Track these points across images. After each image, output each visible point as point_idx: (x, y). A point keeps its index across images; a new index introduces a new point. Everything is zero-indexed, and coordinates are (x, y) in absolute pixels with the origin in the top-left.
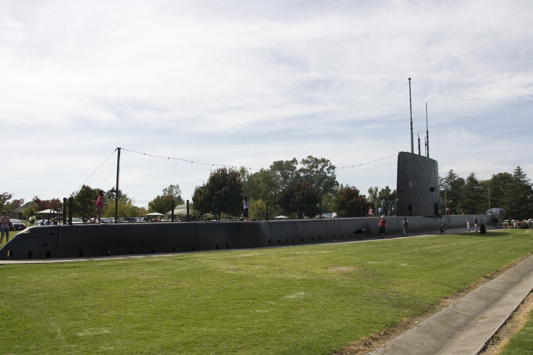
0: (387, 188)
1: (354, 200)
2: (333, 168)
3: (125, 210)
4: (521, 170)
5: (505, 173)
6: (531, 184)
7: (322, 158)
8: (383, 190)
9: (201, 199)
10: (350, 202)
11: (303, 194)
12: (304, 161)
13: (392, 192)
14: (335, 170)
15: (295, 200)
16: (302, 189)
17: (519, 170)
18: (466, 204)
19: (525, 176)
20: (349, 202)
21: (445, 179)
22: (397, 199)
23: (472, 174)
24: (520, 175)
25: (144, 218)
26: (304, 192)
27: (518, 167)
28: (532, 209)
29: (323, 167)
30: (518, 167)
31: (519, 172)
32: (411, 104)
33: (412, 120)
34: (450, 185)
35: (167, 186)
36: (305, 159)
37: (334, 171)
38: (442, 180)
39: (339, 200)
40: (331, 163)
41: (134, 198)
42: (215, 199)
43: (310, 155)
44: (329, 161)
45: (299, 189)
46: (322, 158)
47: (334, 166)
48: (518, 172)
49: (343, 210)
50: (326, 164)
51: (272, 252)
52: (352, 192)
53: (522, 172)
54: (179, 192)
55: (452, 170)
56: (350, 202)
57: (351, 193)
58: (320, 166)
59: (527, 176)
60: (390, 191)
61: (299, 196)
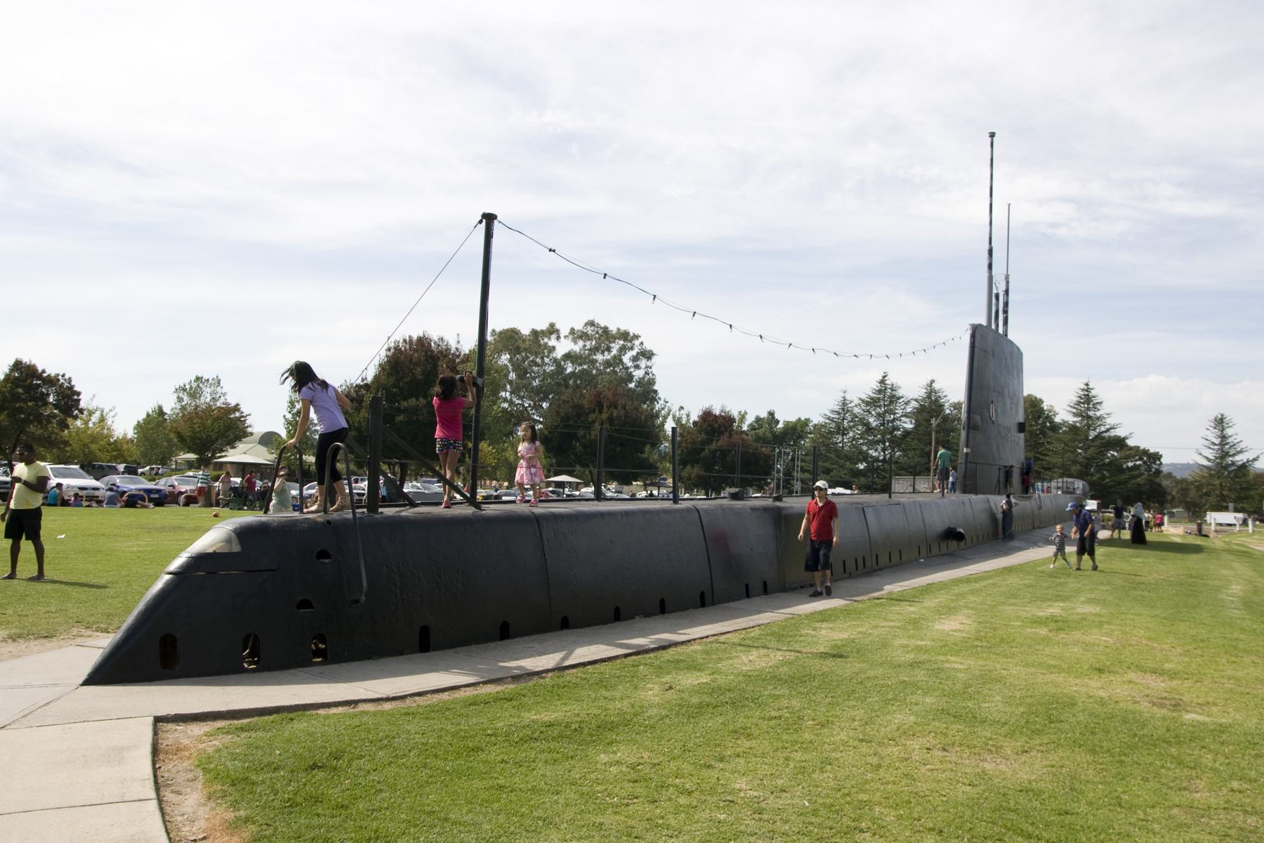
0: (771, 414)
1: (723, 442)
2: (648, 355)
3: (92, 442)
4: (1092, 391)
6: (1109, 424)
7: (618, 329)
8: (758, 419)
9: (362, 420)
10: (713, 446)
11: (611, 420)
12: (574, 333)
13: (780, 425)
16: (607, 407)
17: (1087, 391)
19: (1098, 407)
20: (710, 447)
21: (916, 400)
22: (967, 446)
24: (1088, 404)
25: (126, 466)
26: (615, 414)
27: (1087, 385)
28: (1110, 484)
29: (623, 350)
30: (1087, 385)
31: (1088, 395)
32: (991, 201)
33: (993, 245)
35: (186, 379)
36: (579, 326)
37: (649, 364)
38: (907, 403)
39: (684, 439)
40: (642, 343)
41: (114, 408)
42: (401, 422)
43: (591, 319)
44: (637, 337)
45: (600, 406)
46: (618, 329)
47: (650, 351)
48: (1084, 395)
50: (629, 344)
52: (719, 422)
53: (1094, 397)
54: (220, 397)
55: (933, 381)
56: (713, 446)
57: (717, 422)
58: (615, 348)
59: (1104, 405)
60: (778, 422)
61: (602, 424)
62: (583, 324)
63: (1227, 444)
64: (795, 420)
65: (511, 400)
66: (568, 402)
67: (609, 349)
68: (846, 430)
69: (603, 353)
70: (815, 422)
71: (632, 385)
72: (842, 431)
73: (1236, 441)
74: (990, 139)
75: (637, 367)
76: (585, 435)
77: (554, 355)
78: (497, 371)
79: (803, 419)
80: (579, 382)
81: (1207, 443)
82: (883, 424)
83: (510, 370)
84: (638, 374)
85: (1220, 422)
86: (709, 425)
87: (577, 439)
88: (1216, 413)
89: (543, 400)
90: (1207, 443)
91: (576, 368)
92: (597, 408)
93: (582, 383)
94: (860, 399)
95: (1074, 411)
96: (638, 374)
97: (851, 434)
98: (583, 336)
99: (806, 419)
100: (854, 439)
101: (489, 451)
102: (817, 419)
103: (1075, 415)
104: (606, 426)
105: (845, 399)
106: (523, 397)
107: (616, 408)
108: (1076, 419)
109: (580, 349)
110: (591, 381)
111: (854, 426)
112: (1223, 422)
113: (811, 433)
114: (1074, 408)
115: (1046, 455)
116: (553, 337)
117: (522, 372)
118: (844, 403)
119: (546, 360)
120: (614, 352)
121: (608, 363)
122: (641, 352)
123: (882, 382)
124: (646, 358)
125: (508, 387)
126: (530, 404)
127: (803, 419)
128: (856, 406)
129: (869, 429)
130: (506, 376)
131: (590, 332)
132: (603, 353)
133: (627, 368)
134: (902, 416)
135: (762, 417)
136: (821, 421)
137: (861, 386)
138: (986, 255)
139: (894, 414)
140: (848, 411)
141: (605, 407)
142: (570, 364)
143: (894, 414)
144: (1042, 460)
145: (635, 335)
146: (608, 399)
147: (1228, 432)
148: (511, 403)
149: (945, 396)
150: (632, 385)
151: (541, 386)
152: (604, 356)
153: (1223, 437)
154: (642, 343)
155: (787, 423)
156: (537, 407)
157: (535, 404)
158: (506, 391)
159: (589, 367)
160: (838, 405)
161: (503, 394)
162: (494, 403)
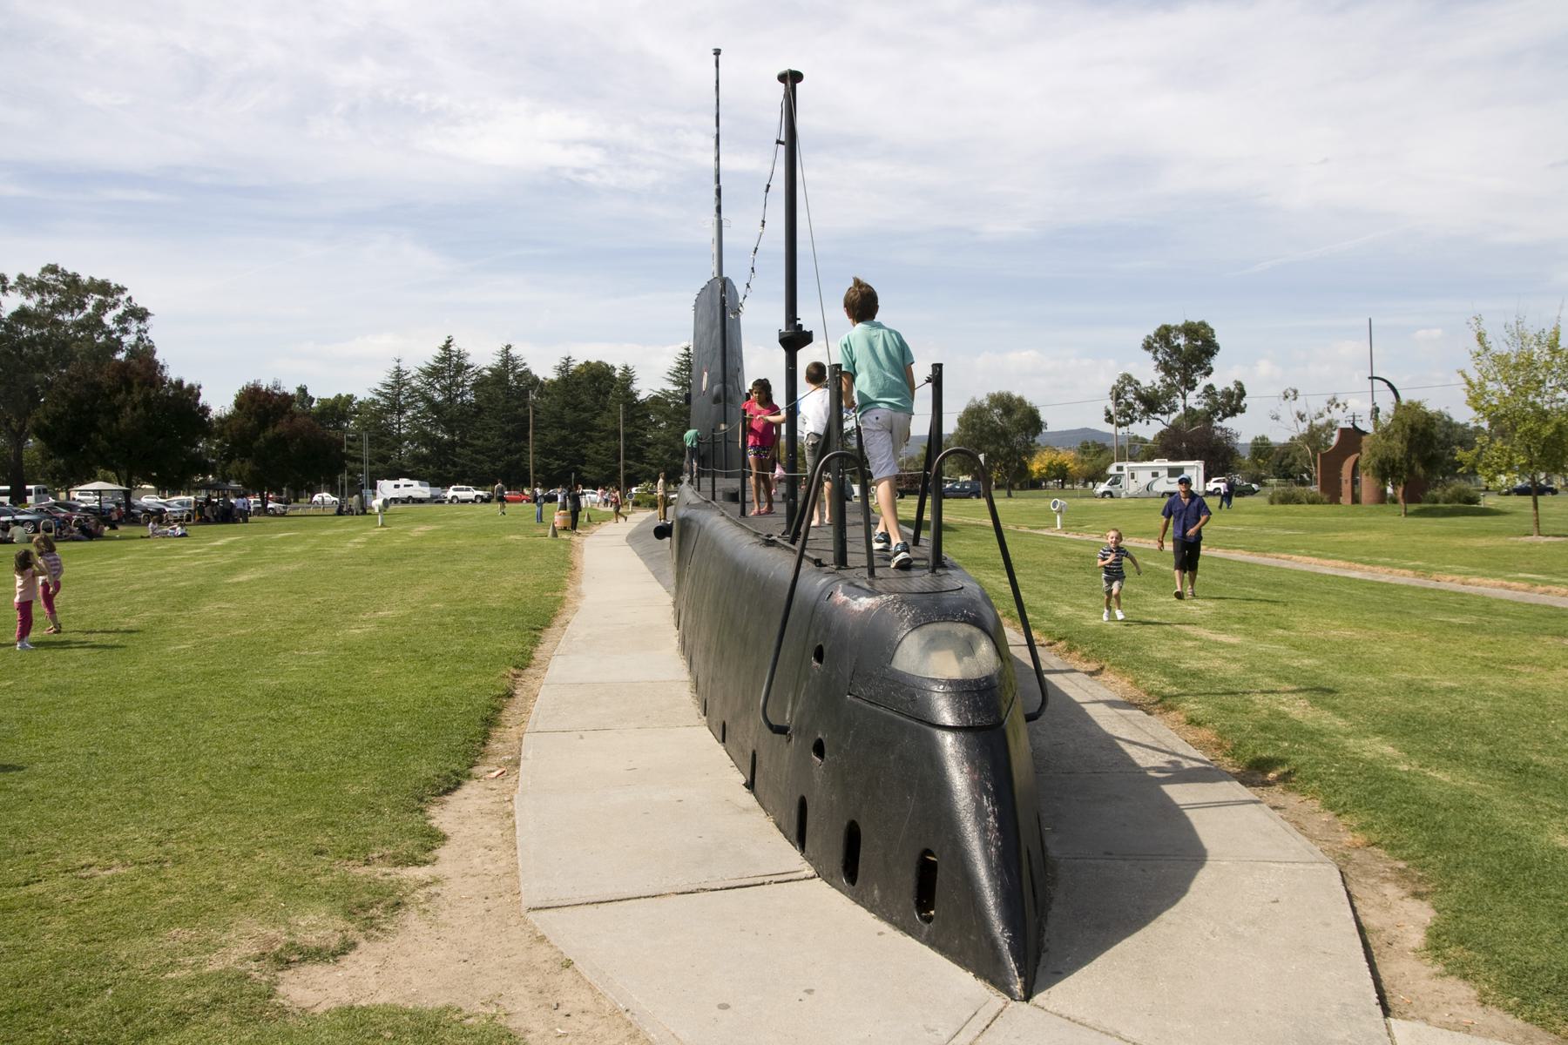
1: (282, 427)
2: (141, 315)
10: (270, 433)
14: (148, 322)
18: (553, 445)
23: (568, 359)
29: (101, 307)
34: (132, 393)
36: (33, 273)
37: (142, 326)
40: (130, 299)
44: (121, 290)
46: (92, 279)
49: (243, 462)
51: (158, 572)
55: (509, 347)
56: (270, 433)
57: (270, 402)
58: (91, 302)
60: (312, 400)
61: (134, 409)
62: (40, 271)
66: (78, 379)
67: (82, 306)
68: (403, 407)
70: (360, 399)
71: (121, 356)
72: (396, 407)
74: (714, 57)
75: (125, 331)
79: (344, 395)
84: (129, 340)
86: (260, 406)
92: (124, 388)
95: (675, 379)
97: (409, 413)
98: (41, 287)
99: (348, 396)
100: (415, 417)
102: (363, 394)
103: (676, 383)
104: (141, 411)
105: (398, 368)
108: (676, 388)
114: (674, 376)
118: (398, 374)
120: (89, 309)
121: (80, 325)
122: (131, 310)
123: (446, 348)
124: (137, 318)
127: (344, 395)
129: (433, 406)
133: (111, 332)
136: (367, 398)
137: (420, 354)
138: (714, 195)
141: (136, 385)
145: (118, 288)
146: (138, 374)
149: (524, 364)
150: (121, 356)
152: (72, 315)
154: (130, 299)
155: (323, 402)
160: (391, 377)
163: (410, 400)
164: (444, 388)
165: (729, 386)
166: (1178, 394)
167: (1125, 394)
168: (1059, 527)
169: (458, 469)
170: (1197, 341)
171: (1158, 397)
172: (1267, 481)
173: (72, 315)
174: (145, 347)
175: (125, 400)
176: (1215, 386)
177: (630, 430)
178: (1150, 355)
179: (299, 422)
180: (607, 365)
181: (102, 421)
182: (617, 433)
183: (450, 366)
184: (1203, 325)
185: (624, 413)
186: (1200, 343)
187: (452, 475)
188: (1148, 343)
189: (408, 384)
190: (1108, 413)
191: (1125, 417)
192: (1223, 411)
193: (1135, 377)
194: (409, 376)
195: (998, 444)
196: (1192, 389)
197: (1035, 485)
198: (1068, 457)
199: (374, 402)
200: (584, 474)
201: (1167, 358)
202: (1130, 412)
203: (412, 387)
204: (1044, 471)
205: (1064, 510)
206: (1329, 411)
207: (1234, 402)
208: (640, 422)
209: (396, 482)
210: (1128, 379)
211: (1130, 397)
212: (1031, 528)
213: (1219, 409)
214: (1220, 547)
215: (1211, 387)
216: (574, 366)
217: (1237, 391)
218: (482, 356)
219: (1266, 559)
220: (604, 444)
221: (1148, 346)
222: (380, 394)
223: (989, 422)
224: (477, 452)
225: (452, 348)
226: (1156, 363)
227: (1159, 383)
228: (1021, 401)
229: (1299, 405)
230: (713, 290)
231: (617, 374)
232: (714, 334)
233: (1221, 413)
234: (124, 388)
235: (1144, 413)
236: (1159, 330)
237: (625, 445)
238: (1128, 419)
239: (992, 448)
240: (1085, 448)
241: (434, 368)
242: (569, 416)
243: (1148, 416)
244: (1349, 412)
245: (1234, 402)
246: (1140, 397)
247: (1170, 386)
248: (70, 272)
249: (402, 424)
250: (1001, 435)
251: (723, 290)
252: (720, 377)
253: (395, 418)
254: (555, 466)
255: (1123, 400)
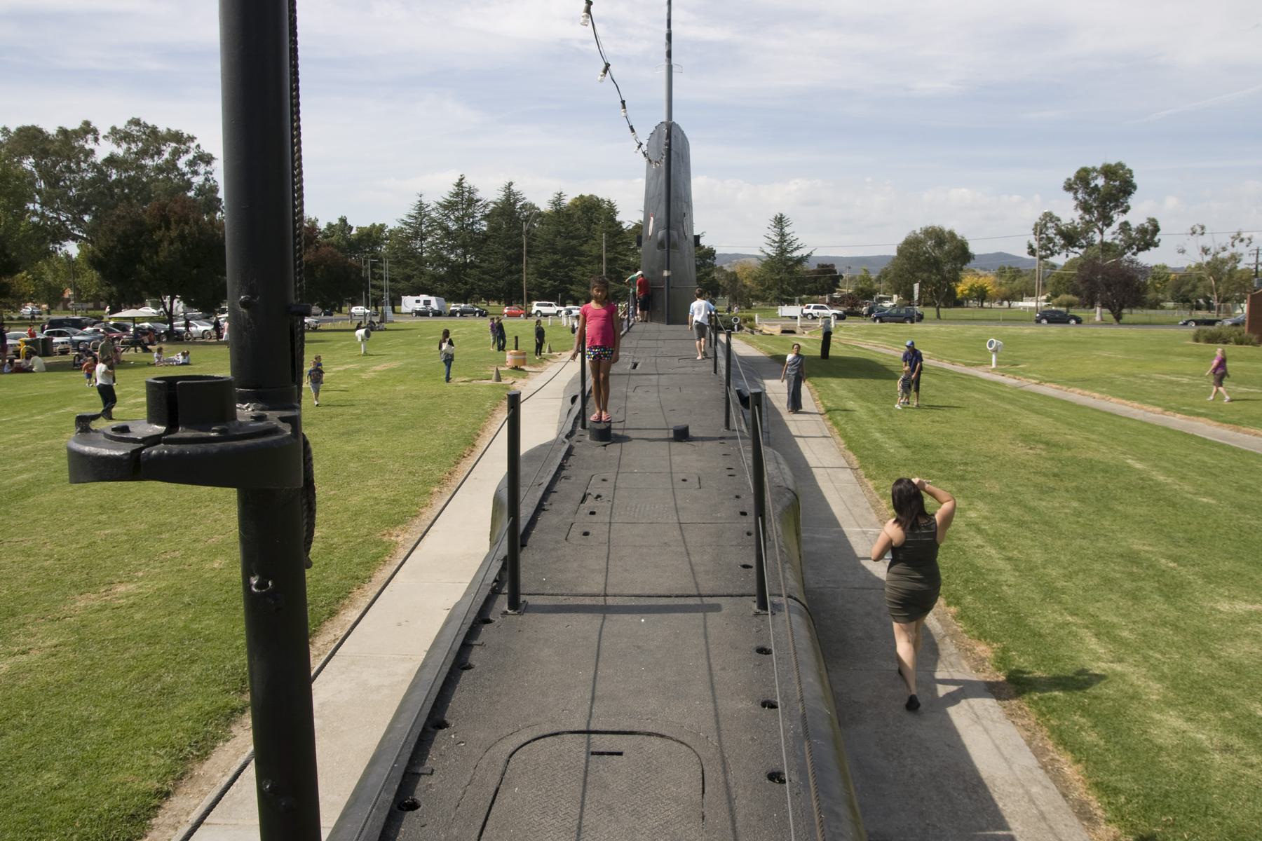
5: (592, 196)
11: (182, 237)
15: (158, 256)
18: (546, 267)
21: (495, 203)
23: (560, 194)
26: (187, 231)
29: (176, 154)
36: (121, 125)
37: (208, 169)
40: (198, 146)
43: (136, 117)
44: (192, 139)
45: (166, 221)
46: (169, 129)
55: (511, 184)
58: (167, 150)
60: (351, 228)
61: (171, 243)
62: (126, 123)
63: (785, 241)
64: (368, 226)
65: (43, 213)
66: (124, 217)
67: (159, 153)
68: (425, 234)
69: (152, 157)
70: (391, 227)
71: (191, 194)
73: (792, 239)
75: (195, 173)
76: (151, 257)
77: (93, 160)
78: (17, 178)
79: (377, 224)
80: (126, 191)
81: (769, 241)
82: (462, 228)
83: (37, 176)
84: (197, 180)
85: (780, 221)
87: (142, 262)
88: (776, 212)
89: (85, 212)
90: (769, 241)
91: (121, 175)
92: (163, 225)
93: (131, 192)
94: (438, 203)
96: (197, 180)
97: (430, 239)
101: (23, 278)
102: (392, 224)
104: (177, 245)
105: (420, 201)
106: (58, 209)
107: (187, 223)
109: (125, 153)
110: (141, 191)
111: (432, 231)
112: (782, 222)
113: (387, 239)
115: (625, 255)
116: (90, 137)
117: (53, 181)
118: (421, 207)
119: (83, 166)
120: (166, 155)
121: (159, 169)
122: (199, 156)
123: (459, 184)
125: (37, 197)
126: (67, 217)
127: (377, 224)
128: (433, 209)
129: (448, 233)
130: (32, 184)
131: (135, 133)
132: (152, 157)
133: (184, 174)
134: (481, 219)
135: (334, 224)
137: (438, 189)
138: (664, 39)
139: (473, 217)
140: (425, 215)
142: (114, 171)
143: (473, 217)
144: (623, 260)
145: (189, 137)
146: (175, 213)
147: (787, 230)
148: (42, 216)
150: (191, 194)
151: (80, 197)
153: (783, 235)
154: (198, 146)
156: (78, 221)
157: (74, 218)
158: (35, 202)
159: (137, 173)
160: (414, 209)
161: (31, 206)
162: (22, 217)
163: (430, 229)
164: (457, 219)
165: (674, 233)
166: (1096, 230)
167: (1047, 229)
168: (994, 366)
169: (468, 287)
170: (1115, 181)
171: (1078, 233)
172: (1164, 304)
173: (154, 161)
174: (211, 187)
175: (163, 235)
176: (1130, 223)
177: (611, 255)
178: (1071, 195)
179: (323, 250)
180: (598, 199)
181: (146, 254)
182: (600, 257)
183: (462, 200)
184: (1121, 166)
185: (606, 241)
186: (1117, 183)
187: (463, 291)
188: (1070, 185)
189: (429, 215)
190: (1030, 246)
191: (1046, 250)
192: (1137, 246)
193: (1056, 214)
194: (429, 208)
195: (931, 272)
196: (1108, 225)
197: (959, 304)
198: (988, 281)
199: (401, 231)
200: (572, 293)
201: (1087, 197)
202: (1051, 245)
203: (431, 218)
204: (967, 292)
205: (999, 350)
206: (1233, 246)
207: (1148, 237)
208: (620, 248)
209: (417, 298)
210: (1049, 217)
211: (1051, 232)
212: (967, 365)
213: (1134, 244)
214: (1179, 411)
215: (1126, 223)
216: (567, 201)
217: (1150, 228)
218: (489, 192)
219: (1241, 435)
220: (589, 267)
221: (1069, 187)
222: (405, 223)
223: (925, 253)
224: (484, 273)
225: (464, 185)
226: (1075, 203)
227: (1077, 220)
228: (952, 235)
229: (1205, 241)
230: (659, 136)
231: (605, 206)
232: (660, 178)
233: (1135, 247)
234: (163, 225)
235: (1063, 247)
236: (1078, 172)
237: (607, 268)
238: (1049, 252)
239: (925, 275)
240: (1001, 272)
241: (449, 202)
242: (560, 243)
243: (1067, 249)
244: (1253, 246)
245: (1148, 237)
246: (1060, 233)
247: (1088, 222)
248: (150, 125)
249: (424, 248)
250: (934, 264)
251: (669, 136)
252: (663, 222)
253: (419, 243)
254: (548, 285)
255: (1044, 236)
